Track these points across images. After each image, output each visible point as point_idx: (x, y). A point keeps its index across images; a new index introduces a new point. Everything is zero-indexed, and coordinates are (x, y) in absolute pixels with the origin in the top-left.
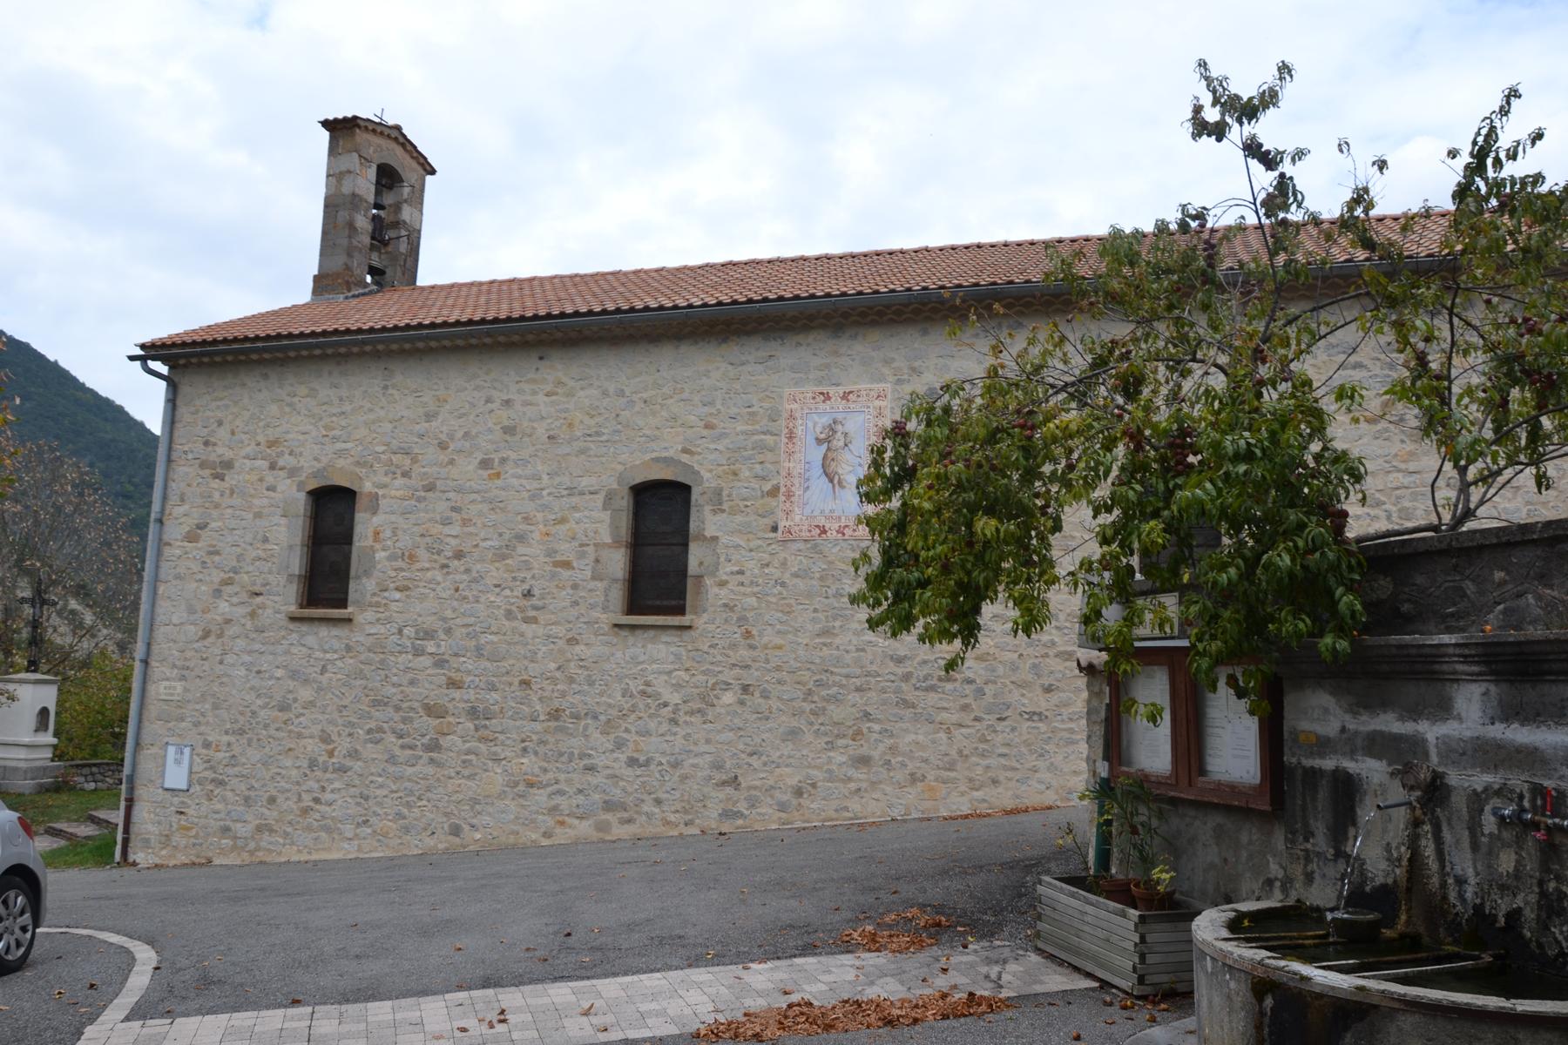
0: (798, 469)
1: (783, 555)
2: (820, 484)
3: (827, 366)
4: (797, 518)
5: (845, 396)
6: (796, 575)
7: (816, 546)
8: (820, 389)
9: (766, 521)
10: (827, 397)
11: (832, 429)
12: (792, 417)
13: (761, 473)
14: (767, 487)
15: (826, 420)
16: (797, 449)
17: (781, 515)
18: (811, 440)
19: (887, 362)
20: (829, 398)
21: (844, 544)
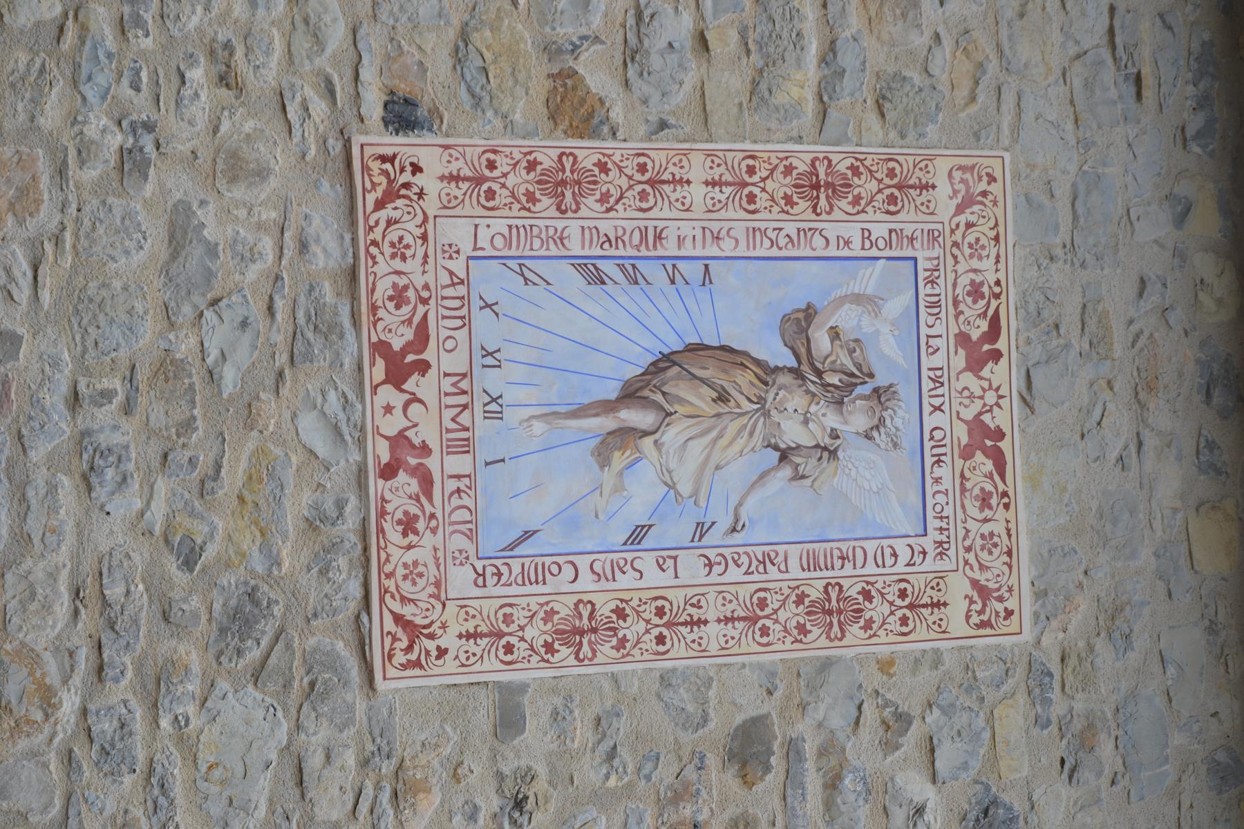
0: (682, 223)
1: (280, 159)
2: (625, 332)
3: (1098, 346)
4: (456, 231)
5: (985, 439)
6: (181, 229)
7: (330, 331)
8: (1011, 323)
9: (441, 66)
10: (981, 353)
11: (849, 383)
12: (902, 189)
13: (656, 42)
14: (597, 76)
15: (888, 353)
16: (768, 218)
17: (473, 145)
18: (803, 284)
19: (1113, 620)
20: (975, 365)
21: (339, 478)
